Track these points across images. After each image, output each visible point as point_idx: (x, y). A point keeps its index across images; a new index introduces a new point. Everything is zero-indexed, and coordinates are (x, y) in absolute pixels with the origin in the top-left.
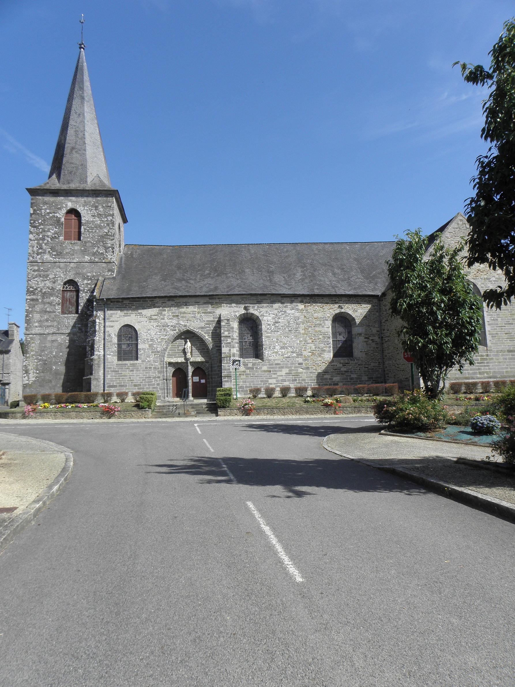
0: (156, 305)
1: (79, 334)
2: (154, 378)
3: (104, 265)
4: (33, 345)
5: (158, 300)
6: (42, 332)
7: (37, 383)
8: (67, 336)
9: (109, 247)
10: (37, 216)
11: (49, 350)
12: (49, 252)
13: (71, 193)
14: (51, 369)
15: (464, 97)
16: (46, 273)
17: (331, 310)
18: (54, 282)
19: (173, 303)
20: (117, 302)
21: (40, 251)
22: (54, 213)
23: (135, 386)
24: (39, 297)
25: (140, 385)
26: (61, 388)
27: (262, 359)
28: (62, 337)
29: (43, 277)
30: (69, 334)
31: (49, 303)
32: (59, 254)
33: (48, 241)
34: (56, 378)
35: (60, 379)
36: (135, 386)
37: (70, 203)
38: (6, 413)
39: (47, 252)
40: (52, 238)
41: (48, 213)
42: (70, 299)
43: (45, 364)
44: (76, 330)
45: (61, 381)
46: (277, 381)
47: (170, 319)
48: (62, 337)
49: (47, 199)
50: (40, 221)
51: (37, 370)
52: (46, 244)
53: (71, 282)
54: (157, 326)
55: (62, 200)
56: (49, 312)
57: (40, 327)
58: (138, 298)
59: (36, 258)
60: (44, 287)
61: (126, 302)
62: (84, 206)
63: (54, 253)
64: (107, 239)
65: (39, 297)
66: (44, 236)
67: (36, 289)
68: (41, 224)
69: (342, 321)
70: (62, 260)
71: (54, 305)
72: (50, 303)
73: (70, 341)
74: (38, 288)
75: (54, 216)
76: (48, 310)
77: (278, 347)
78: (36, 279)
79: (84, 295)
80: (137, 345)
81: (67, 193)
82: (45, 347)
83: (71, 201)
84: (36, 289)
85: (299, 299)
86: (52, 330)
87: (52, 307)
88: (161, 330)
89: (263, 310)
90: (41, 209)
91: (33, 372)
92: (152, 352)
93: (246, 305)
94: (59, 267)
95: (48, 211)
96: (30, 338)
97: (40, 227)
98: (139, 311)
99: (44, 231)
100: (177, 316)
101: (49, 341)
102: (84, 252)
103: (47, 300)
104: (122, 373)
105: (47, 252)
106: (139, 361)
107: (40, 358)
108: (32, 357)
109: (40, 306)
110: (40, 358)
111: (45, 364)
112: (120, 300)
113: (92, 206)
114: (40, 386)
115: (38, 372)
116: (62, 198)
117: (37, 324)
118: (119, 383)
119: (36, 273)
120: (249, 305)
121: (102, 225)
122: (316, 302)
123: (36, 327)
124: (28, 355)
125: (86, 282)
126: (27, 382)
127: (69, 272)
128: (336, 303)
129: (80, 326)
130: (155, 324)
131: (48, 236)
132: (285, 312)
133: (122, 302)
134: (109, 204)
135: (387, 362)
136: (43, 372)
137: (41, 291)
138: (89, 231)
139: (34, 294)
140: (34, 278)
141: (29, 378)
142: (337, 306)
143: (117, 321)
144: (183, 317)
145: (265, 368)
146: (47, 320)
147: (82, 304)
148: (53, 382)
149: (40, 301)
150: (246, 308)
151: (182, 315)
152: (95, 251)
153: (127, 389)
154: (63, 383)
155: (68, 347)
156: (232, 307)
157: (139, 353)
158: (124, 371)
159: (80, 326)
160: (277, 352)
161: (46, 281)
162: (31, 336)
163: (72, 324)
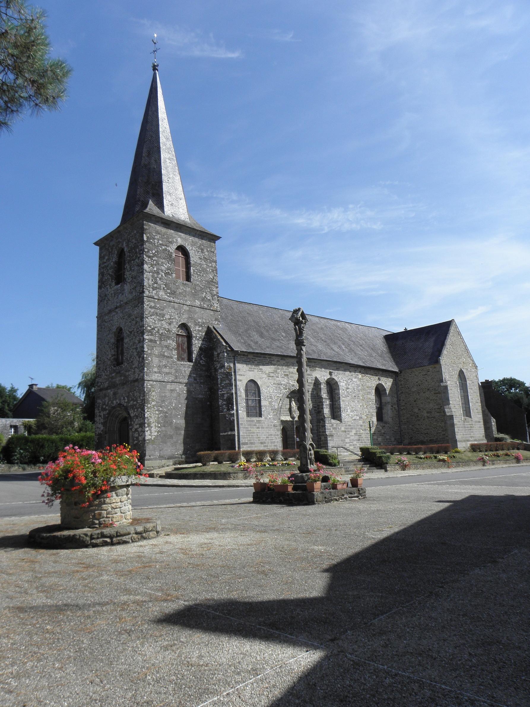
0: (273, 362)
1: (194, 385)
2: (275, 435)
3: (212, 313)
4: (153, 393)
5: (274, 357)
6: (160, 378)
7: (159, 438)
8: (185, 386)
9: (215, 295)
10: (151, 245)
11: (168, 401)
12: (164, 288)
13: (180, 228)
14: (172, 423)
15: (204, 195)
16: (161, 312)
17: (373, 381)
18: (170, 324)
19: (284, 362)
20: (244, 355)
21: (155, 285)
22: (166, 246)
23: (262, 443)
24: (157, 339)
25: (265, 442)
26: (182, 445)
27: (340, 420)
28: (180, 387)
29: (159, 317)
30: (187, 384)
31: (166, 346)
32: (173, 293)
33: (162, 275)
34: (177, 434)
35: (180, 434)
36: (262, 443)
37: (180, 239)
38: (225, 473)
39: (162, 288)
40: (167, 274)
41: (161, 244)
42: (181, 345)
43: (166, 417)
44: (192, 380)
45: (182, 437)
46: (350, 440)
47: (283, 377)
48: (180, 387)
49: (159, 228)
50: (154, 252)
51: (158, 423)
52: (160, 279)
53: (184, 326)
54: (274, 384)
55: (172, 234)
56: (168, 357)
57: (159, 373)
58: (261, 354)
59: (152, 292)
60: (161, 327)
61: (250, 356)
62: (192, 246)
63: (169, 291)
64: (213, 285)
65: (157, 339)
66: (158, 269)
67: (153, 329)
68: (154, 255)
69: (379, 391)
70: (176, 301)
71: (171, 350)
72: (167, 347)
73: (188, 391)
74: (156, 327)
75: (166, 250)
76: (166, 354)
77: (349, 411)
78: (153, 317)
79: (196, 342)
80: (260, 401)
81: (177, 227)
82: (165, 396)
83: (180, 237)
84: (153, 329)
85: (359, 369)
86: (171, 378)
87: (169, 351)
88: (277, 387)
89: (340, 376)
90: (154, 239)
91: (155, 426)
92: (272, 410)
93: (332, 371)
94: (174, 307)
95: (160, 242)
96: (151, 385)
97: (154, 259)
98: (261, 367)
99: (158, 264)
100: (287, 375)
101: (168, 390)
102: (194, 295)
103: (164, 343)
104: (251, 430)
105: (162, 288)
106: (263, 418)
107: (161, 409)
108: (153, 407)
109: (158, 348)
110: (161, 409)
111: (166, 417)
112: (246, 354)
113: (199, 247)
114: (162, 442)
115: (159, 425)
116: (173, 231)
117: (156, 370)
118: (249, 440)
119: (152, 310)
120: (334, 371)
121: (208, 270)
122: (367, 374)
123: (155, 372)
124: (149, 405)
125: (197, 328)
126: (150, 437)
127: (183, 314)
128: (377, 376)
129: (195, 375)
130: (272, 382)
131: (162, 271)
132: (352, 379)
133: (247, 356)
134: (213, 250)
135: (403, 427)
136: (164, 426)
137: (158, 332)
138: (197, 274)
139: (152, 335)
140: (151, 316)
141: (151, 433)
142: (377, 378)
143: (244, 375)
144: (291, 377)
145: (343, 429)
146: (165, 366)
147: (195, 352)
148: (174, 437)
149: (158, 342)
150: (330, 374)
151: (291, 375)
152: (203, 296)
153: (255, 446)
154: (184, 439)
155: (186, 399)
156: (322, 371)
157: (263, 410)
158: (252, 428)
159: (195, 375)
160: (349, 415)
161: (162, 320)
162: (151, 382)
163: (188, 373)
